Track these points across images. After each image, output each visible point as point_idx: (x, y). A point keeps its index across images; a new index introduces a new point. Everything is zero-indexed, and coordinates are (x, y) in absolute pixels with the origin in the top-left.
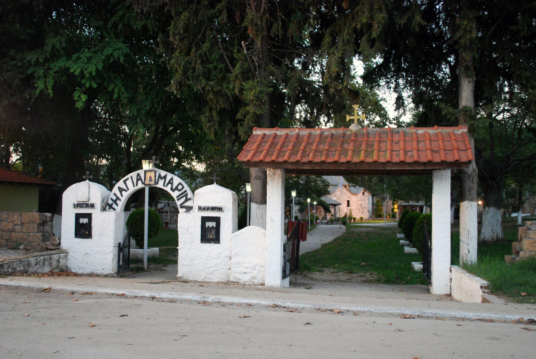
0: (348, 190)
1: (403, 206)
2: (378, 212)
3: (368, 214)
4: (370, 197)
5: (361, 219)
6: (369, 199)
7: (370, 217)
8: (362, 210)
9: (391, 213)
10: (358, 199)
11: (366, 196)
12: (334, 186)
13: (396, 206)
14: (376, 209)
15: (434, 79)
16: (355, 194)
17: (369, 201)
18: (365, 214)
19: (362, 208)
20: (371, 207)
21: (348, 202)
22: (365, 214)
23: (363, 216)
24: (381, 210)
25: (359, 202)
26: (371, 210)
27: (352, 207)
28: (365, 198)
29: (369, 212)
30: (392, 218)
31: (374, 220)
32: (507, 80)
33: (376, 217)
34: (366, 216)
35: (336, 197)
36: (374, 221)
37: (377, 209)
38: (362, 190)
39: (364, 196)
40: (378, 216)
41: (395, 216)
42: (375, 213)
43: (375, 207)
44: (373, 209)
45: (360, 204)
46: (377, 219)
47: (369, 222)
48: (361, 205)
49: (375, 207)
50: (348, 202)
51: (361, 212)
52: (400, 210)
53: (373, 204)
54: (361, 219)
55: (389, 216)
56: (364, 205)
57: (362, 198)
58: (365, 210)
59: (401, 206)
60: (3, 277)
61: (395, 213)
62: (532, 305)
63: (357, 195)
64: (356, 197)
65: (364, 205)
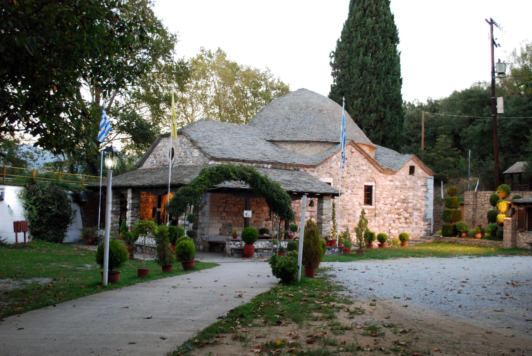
0: (367, 157)
1: (525, 204)
2: (451, 222)
3: (422, 225)
4: (431, 182)
5: (403, 238)
6: (425, 185)
7: (429, 234)
8: (407, 215)
9: (487, 226)
10: (398, 183)
11: (419, 178)
12: (330, 146)
13: (503, 206)
14: (447, 213)
15: (107, 86)
16: (389, 171)
17: (426, 192)
18: (414, 225)
19: (406, 210)
20: (431, 208)
21: (368, 190)
22: (414, 225)
23: (407, 231)
24: (458, 216)
25: (398, 191)
26: (430, 216)
27: (380, 205)
28: (415, 182)
29: (425, 219)
30: (489, 238)
31: (438, 242)
32: (63, 107)
33: (445, 234)
34: (417, 232)
35: (331, 176)
36: (439, 248)
37: (449, 212)
38: (409, 160)
39: (413, 178)
40: (450, 232)
41: (502, 233)
42: (443, 223)
43: (443, 208)
44: (435, 212)
45: (402, 197)
46: (447, 239)
47: (424, 248)
48: (404, 201)
49: (443, 208)
50: (368, 190)
51: (403, 220)
52: (516, 216)
53: (437, 201)
54: (403, 238)
55: (483, 233)
56: (413, 202)
57: (408, 182)
58: (416, 213)
59: (518, 204)
60: (351, 2)
61: (502, 225)
62: (381, 261)
63: (394, 173)
64: (390, 177)
65: (413, 202)
